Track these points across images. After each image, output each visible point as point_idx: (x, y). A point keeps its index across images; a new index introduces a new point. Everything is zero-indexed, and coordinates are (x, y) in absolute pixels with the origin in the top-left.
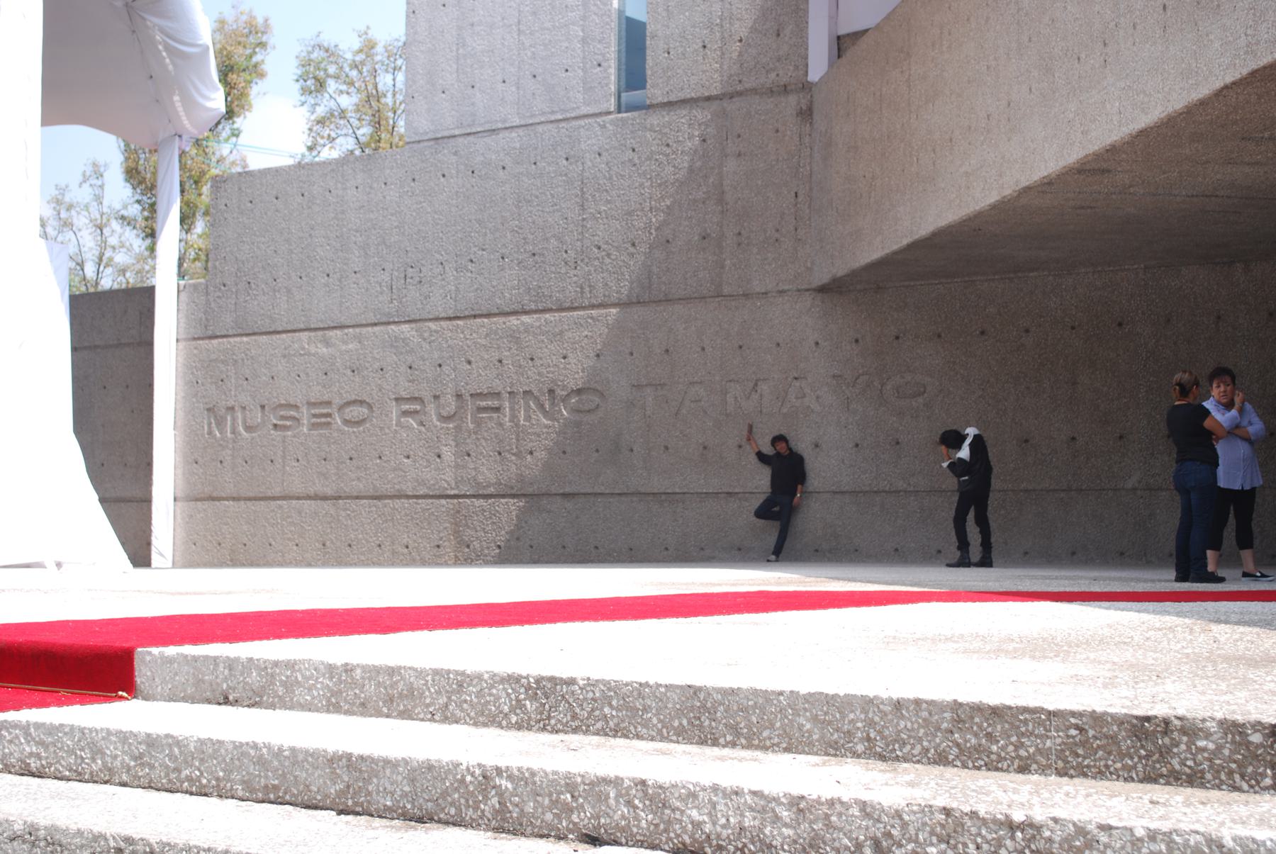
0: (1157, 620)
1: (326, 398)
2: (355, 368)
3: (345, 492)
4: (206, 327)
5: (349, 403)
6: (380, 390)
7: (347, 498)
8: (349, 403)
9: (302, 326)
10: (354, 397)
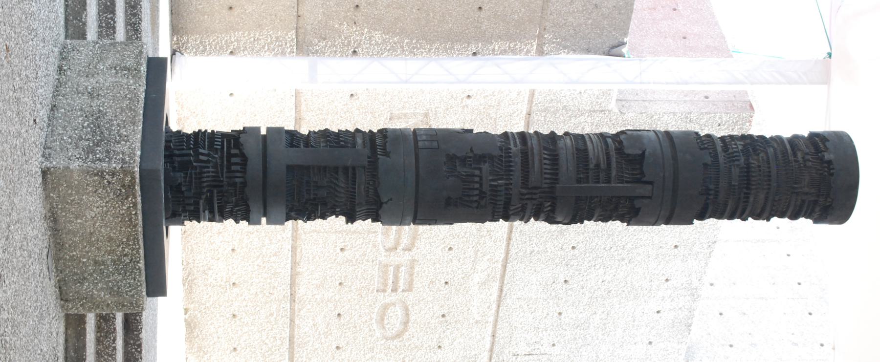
0: (398, 124)
1: (417, 284)
2: (447, 318)
3: (300, 310)
4: (546, 110)
5: (406, 309)
6: (416, 347)
7: (292, 309)
8: (406, 309)
9: (513, 251)
10: (412, 318)
